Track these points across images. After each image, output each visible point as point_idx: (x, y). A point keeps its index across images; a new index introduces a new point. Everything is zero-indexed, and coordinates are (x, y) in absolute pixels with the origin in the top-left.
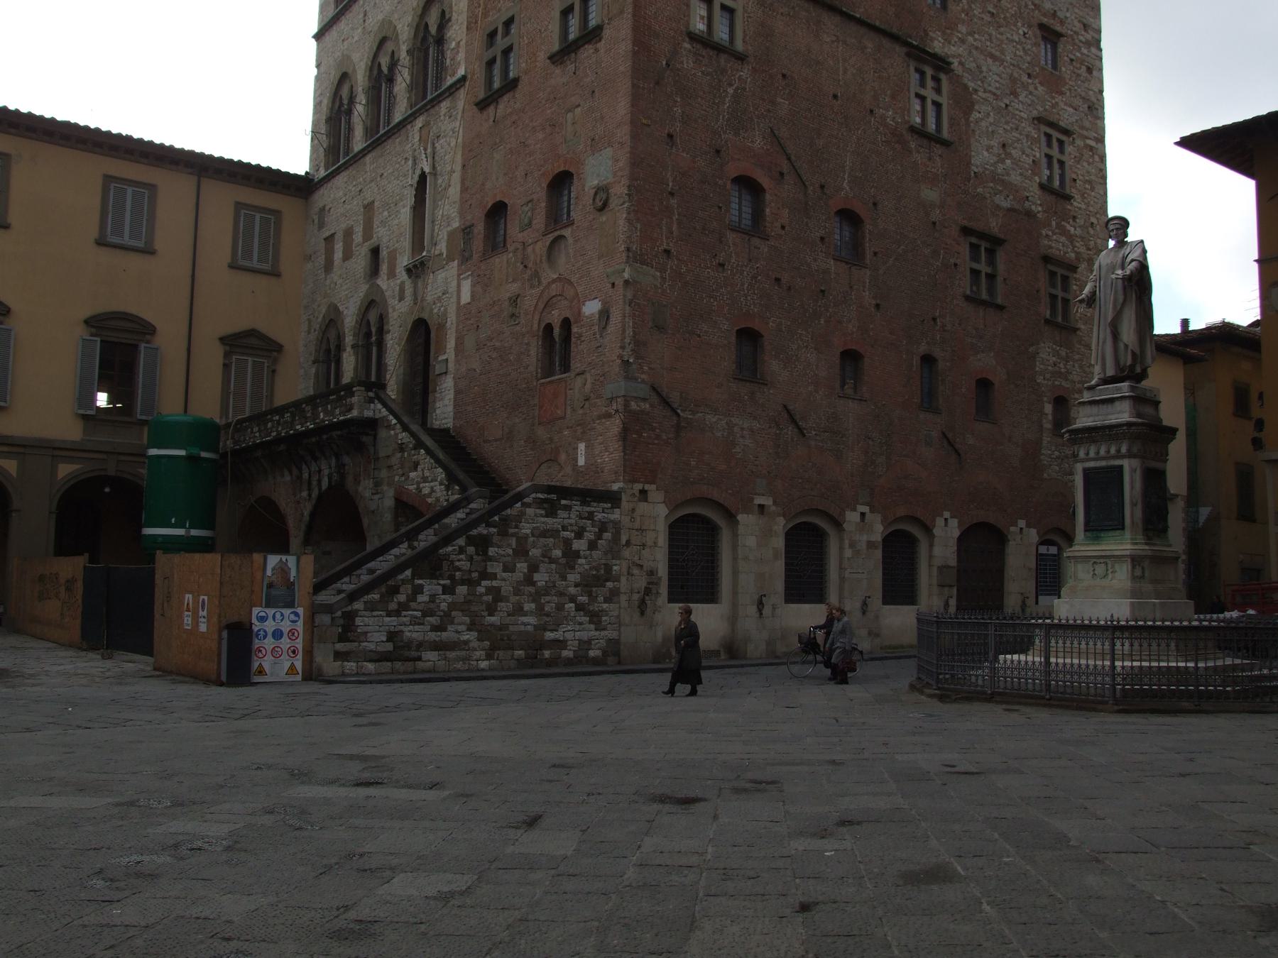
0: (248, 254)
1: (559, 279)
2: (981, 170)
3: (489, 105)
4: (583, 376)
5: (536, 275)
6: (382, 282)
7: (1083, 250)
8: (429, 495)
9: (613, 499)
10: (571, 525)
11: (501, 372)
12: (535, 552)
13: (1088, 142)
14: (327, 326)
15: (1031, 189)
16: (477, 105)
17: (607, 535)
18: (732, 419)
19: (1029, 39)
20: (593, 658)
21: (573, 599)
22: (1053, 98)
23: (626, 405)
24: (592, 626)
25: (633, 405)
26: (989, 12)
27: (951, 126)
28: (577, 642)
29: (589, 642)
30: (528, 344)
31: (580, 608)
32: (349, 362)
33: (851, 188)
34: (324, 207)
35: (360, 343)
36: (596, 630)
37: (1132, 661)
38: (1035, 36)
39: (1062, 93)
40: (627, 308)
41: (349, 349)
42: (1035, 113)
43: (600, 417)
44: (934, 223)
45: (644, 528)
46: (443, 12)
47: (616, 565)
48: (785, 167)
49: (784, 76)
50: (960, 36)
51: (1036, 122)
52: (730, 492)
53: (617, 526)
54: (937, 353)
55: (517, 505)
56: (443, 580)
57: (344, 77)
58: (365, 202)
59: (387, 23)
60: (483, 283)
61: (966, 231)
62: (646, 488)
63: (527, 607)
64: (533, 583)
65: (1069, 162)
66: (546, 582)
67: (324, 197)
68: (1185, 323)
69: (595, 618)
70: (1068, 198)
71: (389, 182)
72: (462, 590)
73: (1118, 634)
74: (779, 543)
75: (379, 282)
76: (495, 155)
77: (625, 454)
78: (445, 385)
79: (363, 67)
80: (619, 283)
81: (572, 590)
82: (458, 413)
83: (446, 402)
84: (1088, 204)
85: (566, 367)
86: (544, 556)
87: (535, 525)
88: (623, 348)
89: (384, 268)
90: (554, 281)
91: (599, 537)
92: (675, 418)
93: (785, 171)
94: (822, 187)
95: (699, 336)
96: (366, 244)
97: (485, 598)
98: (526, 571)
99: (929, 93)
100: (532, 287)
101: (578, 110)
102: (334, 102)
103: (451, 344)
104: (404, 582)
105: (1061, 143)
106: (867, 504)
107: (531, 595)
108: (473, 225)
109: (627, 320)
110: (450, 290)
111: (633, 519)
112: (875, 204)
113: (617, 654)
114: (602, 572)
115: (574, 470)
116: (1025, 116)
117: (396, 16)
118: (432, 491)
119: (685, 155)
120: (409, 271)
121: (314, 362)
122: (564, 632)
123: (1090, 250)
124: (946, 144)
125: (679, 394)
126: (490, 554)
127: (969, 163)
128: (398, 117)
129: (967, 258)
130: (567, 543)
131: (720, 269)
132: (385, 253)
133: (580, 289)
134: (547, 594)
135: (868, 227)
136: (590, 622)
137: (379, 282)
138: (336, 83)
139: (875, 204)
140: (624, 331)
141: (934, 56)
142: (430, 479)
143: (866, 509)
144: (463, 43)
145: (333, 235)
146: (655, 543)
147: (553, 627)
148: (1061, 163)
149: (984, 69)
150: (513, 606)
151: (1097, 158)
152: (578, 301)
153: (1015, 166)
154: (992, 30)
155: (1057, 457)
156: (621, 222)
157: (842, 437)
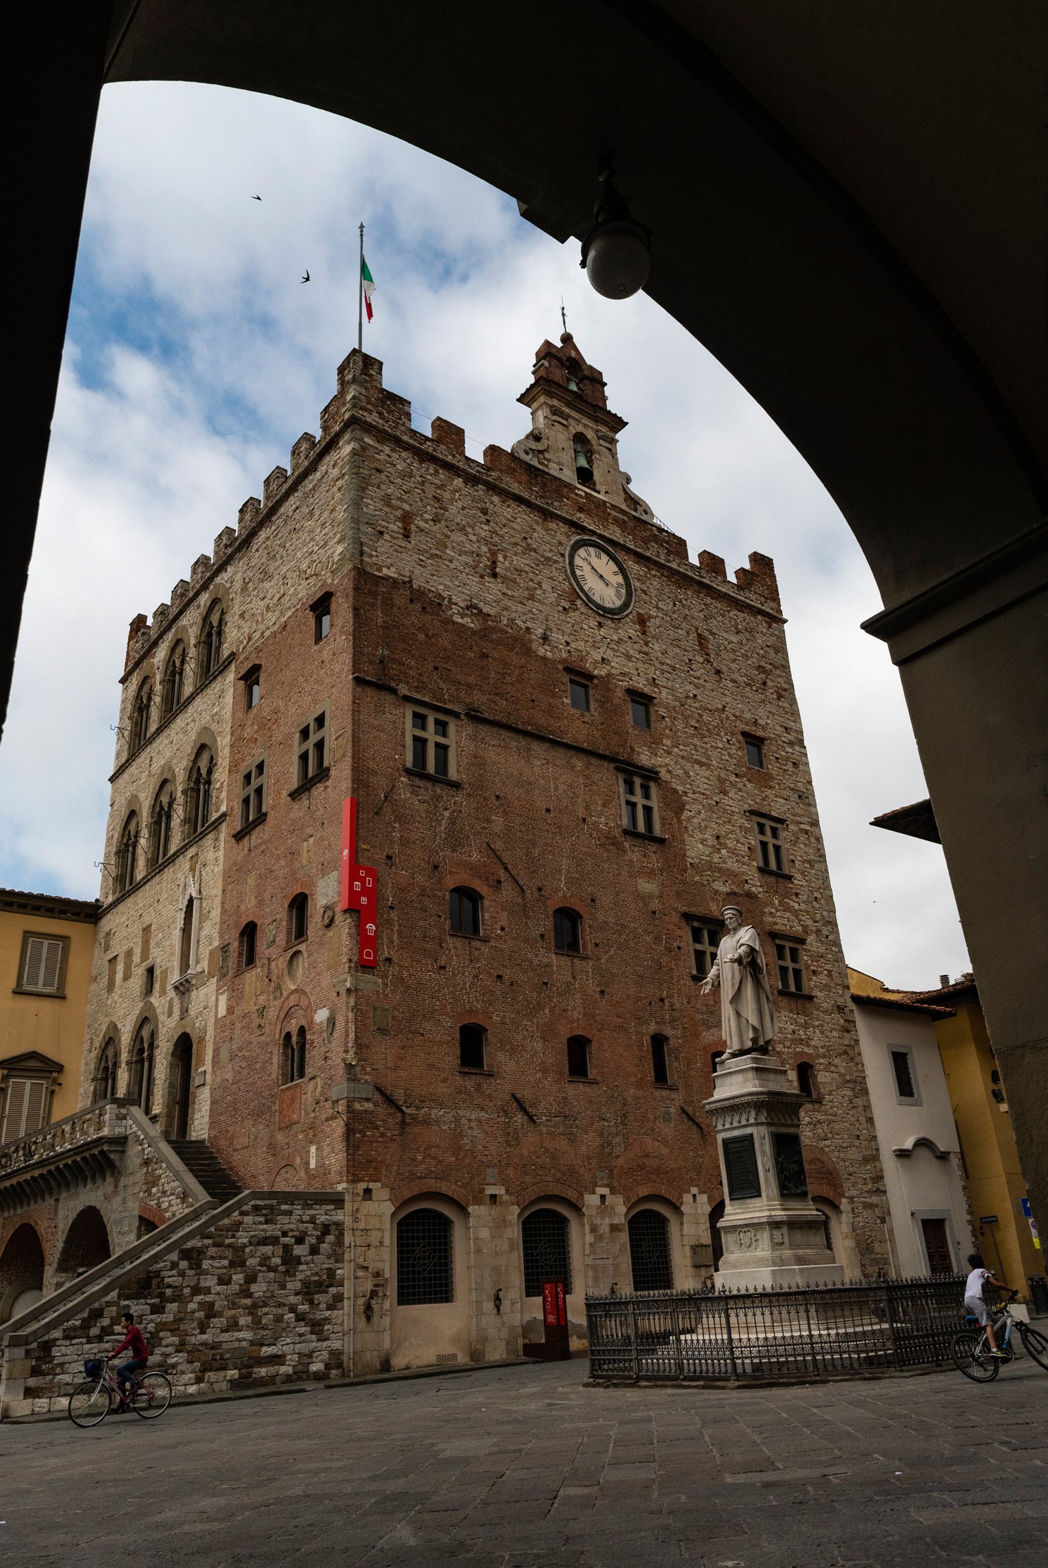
0: (33, 979)
1: (296, 991)
2: (696, 860)
3: (244, 836)
4: (314, 1081)
5: (279, 987)
6: (154, 1000)
7: (810, 923)
8: (166, 1210)
9: (338, 1201)
10: (292, 1230)
11: (249, 1081)
12: (251, 1262)
13: (802, 826)
14: (107, 1044)
15: (749, 873)
16: (234, 836)
17: (330, 1238)
18: (459, 1111)
19: (734, 745)
20: (315, 1372)
21: (293, 1309)
22: (763, 792)
23: (349, 1108)
24: (314, 1337)
25: (357, 1106)
26: (692, 726)
27: (663, 825)
28: (297, 1356)
29: (310, 1355)
30: (271, 1053)
31: (300, 1318)
32: (123, 1077)
33: (568, 888)
34: (110, 931)
35: (134, 1059)
36: (318, 1340)
37: (854, 1326)
38: (739, 742)
39: (771, 787)
40: (350, 1014)
41: (123, 1065)
42: (746, 807)
43: (327, 1120)
44: (654, 912)
45: (369, 1227)
46: (212, 758)
47: (339, 1269)
48: (502, 875)
49: (498, 797)
50: (665, 748)
51: (747, 814)
52: (459, 1184)
53: (339, 1225)
54: (668, 1031)
55: (235, 1214)
56: (151, 1299)
57: (132, 814)
58: (144, 925)
59: (168, 767)
60: (236, 997)
61: (687, 917)
62: (370, 1187)
63: (242, 1321)
64: (250, 1295)
65: (785, 846)
66: (264, 1292)
67: (108, 923)
68: (944, 979)
69: (317, 1327)
70: (789, 878)
71: (164, 907)
72: (172, 1307)
73: (731, 1304)
74: (515, 1232)
75: (152, 1000)
76: (248, 880)
77: (348, 1155)
78: (203, 1096)
79: (148, 805)
80: (343, 992)
81: (293, 1299)
82: (213, 1124)
83: (204, 1113)
84: (809, 881)
85: (302, 1075)
86: (261, 1265)
87: (253, 1233)
88: (346, 1051)
89: (157, 986)
90: (292, 992)
91: (321, 1240)
92: (399, 1115)
93: (502, 879)
94: (540, 890)
95: (422, 1035)
96: (144, 964)
97: (197, 1315)
98: (242, 1282)
99: (638, 799)
100: (275, 999)
101: (311, 840)
102: (123, 836)
103: (209, 1056)
104: (109, 1304)
105: (774, 831)
106: (607, 1186)
107: (248, 1308)
108: (229, 944)
109: (350, 1025)
110: (210, 1005)
111: (356, 1220)
112: (593, 900)
113: (340, 1366)
114: (325, 1277)
115: (306, 1173)
116: (737, 810)
117: (175, 761)
118: (170, 1205)
119: (404, 873)
120: (176, 988)
121: (93, 1080)
122: (282, 1346)
123: (817, 922)
124: (661, 841)
125: (402, 1091)
126: (204, 1267)
127: (685, 855)
128: (173, 849)
129: (691, 940)
130: (287, 1248)
131: (442, 972)
132: (158, 972)
133: (312, 999)
134: (266, 1305)
135: (587, 921)
136: (312, 1333)
137: (152, 1000)
138: (125, 820)
139: (593, 900)
140: (347, 1036)
141: (642, 768)
142: (168, 1193)
143: (605, 1191)
144: (225, 784)
145: (115, 957)
146: (381, 1242)
147: (271, 1341)
148: (777, 848)
149: (691, 773)
150: (228, 1322)
151: (813, 840)
152: (310, 1010)
153: (730, 855)
154: (696, 741)
155: (809, 1123)
156: (344, 936)
157: (574, 1121)
